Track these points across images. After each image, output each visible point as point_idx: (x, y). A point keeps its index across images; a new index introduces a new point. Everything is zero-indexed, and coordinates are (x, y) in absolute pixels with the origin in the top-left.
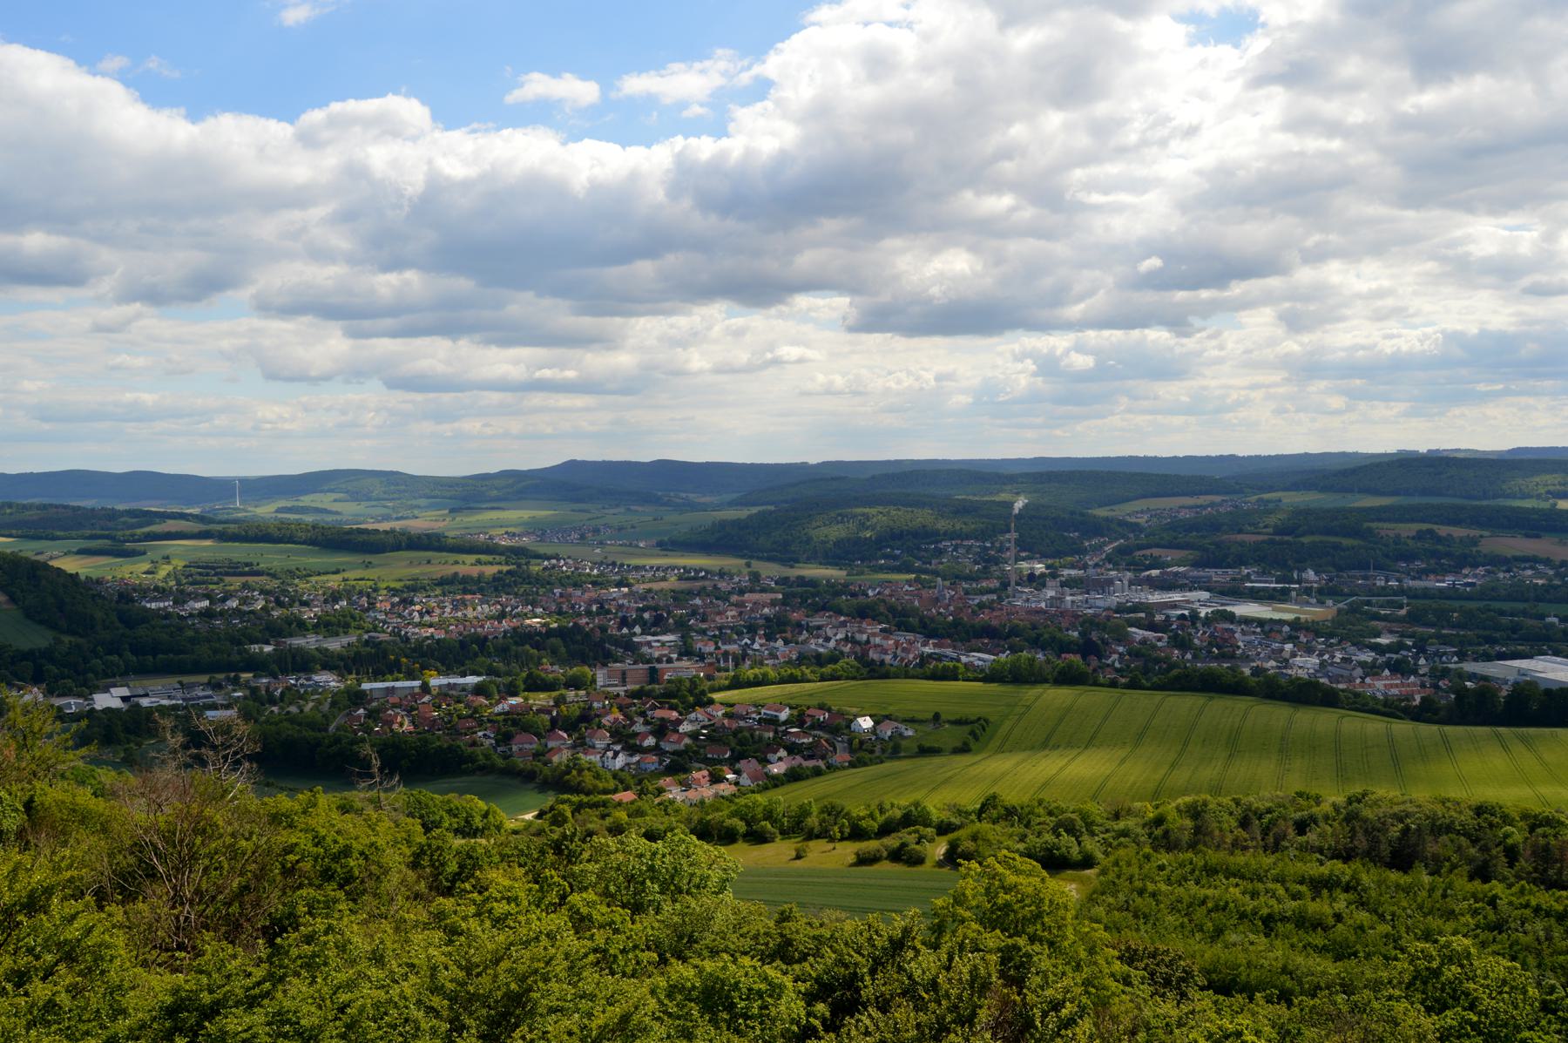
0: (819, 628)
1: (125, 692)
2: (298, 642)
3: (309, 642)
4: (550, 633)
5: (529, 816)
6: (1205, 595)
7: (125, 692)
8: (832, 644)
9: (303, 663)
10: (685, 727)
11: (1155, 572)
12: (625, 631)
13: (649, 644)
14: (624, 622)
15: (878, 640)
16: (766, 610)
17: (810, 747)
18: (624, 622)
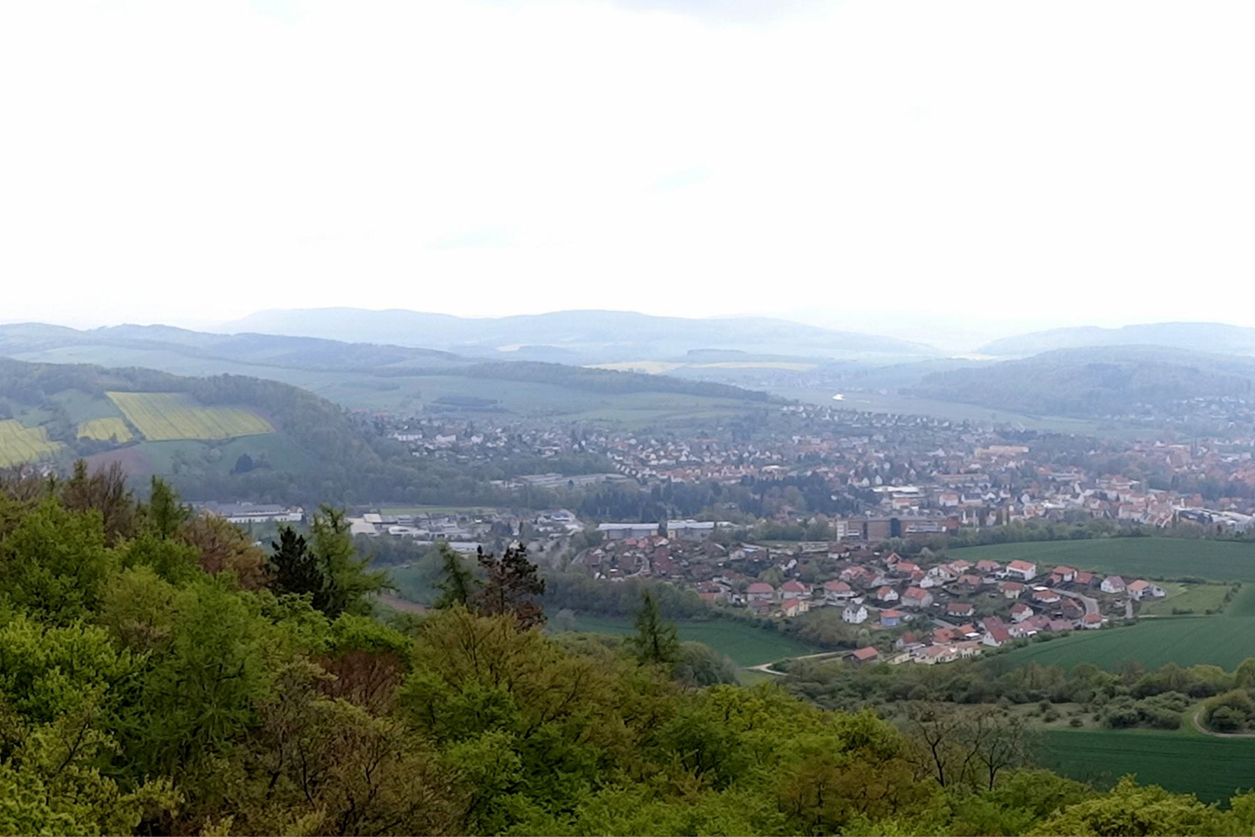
0: (1066, 483)
1: (376, 518)
2: (538, 481)
3: (549, 482)
4: (788, 481)
5: (763, 668)
7: (376, 518)
8: (1080, 500)
9: (543, 502)
10: (927, 582)
12: (866, 482)
13: (890, 495)
14: (865, 473)
15: (1128, 497)
16: (1012, 464)
17: (1057, 606)
18: (865, 473)
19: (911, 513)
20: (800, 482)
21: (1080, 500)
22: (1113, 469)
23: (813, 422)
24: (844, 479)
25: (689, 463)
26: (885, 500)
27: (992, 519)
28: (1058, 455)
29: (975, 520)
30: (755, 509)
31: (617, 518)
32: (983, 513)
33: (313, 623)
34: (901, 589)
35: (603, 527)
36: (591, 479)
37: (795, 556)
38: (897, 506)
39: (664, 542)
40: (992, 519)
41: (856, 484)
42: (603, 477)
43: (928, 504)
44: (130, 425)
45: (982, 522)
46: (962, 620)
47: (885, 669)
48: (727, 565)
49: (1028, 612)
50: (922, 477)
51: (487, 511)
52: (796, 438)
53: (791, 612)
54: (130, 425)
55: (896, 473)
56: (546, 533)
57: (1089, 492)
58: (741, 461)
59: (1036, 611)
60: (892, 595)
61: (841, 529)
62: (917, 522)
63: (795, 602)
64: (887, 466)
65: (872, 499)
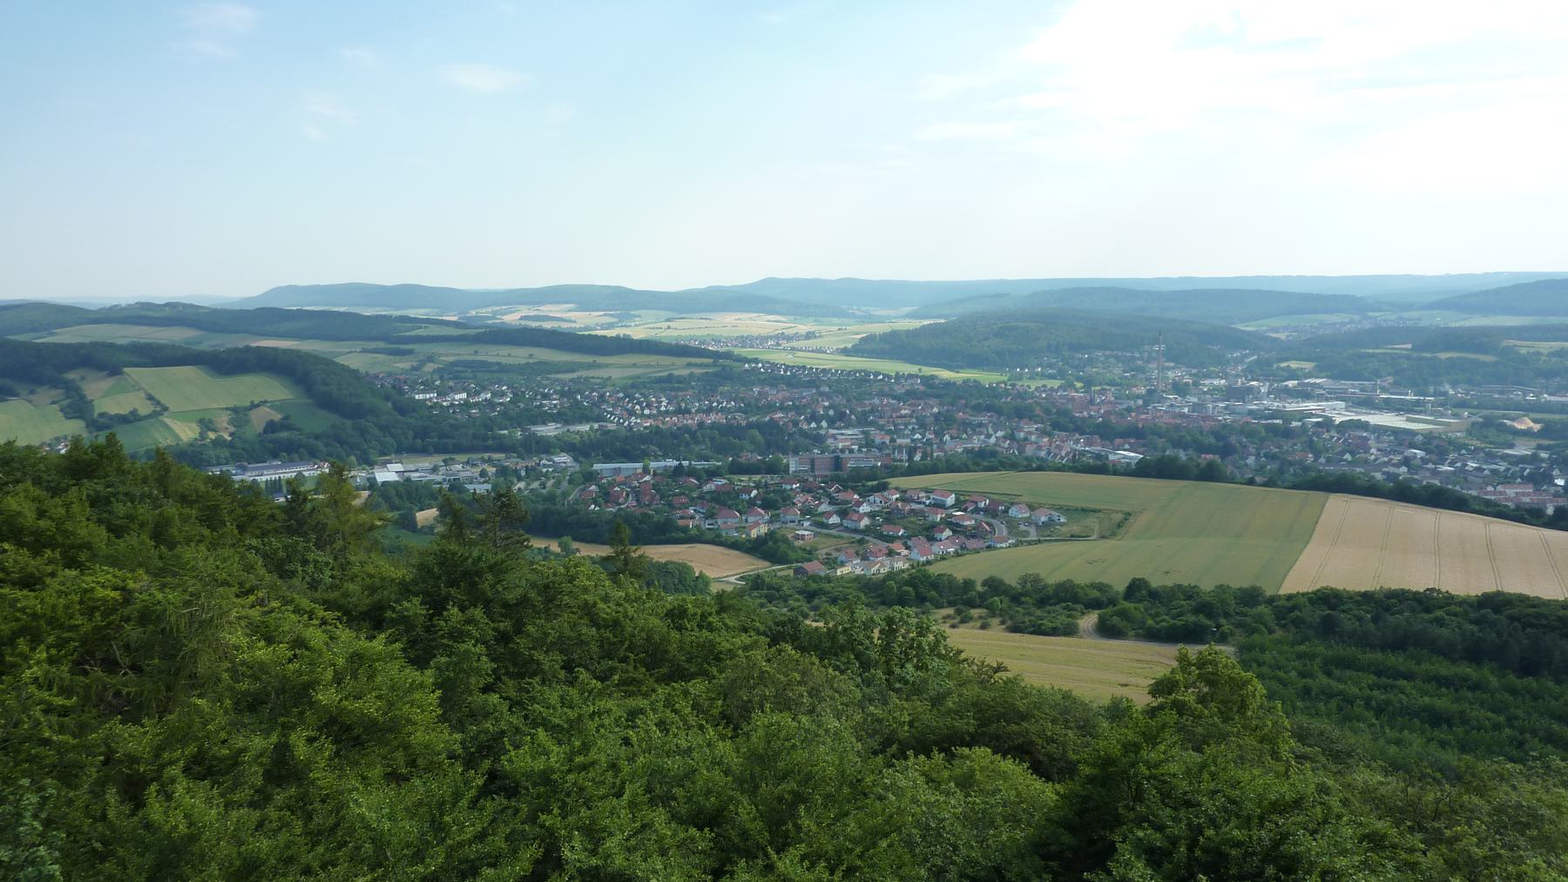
3: (549, 430)
6: (1342, 404)
7: (399, 467)
8: (993, 440)
10: (865, 508)
11: (1291, 384)
12: (813, 425)
13: (834, 436)
14: (814, 417)
19: (851, 451)
20: (758, 426)
21: (993, 440)
22: (1022, 413)
23: (773, 376)
24: (796, 424)
25: (667, 412)
26: (830, 441)
27: (917, 458)
28: (975, 402)
29: (905, 457)
30: (721, 449)
31: (608, 459)
32: (911, 451)
33: (316, 562)
34: (843, 514)
35: (597, 467)
36: (585, 428)
37: (757, 487)
38: (840, 445)
39: (647, 478)
40: (917, 458)
41: (805, 427)
42: (596, 426)
43: (868, 444)
44: (150, 398)
45: (910, 459)
46: (891, 539)
47: (828, 580)
48: (701, 497)
49: (948, 533)
50: (862, 421)
51: (496, 456)
52: (756, 390)
53: (754, 533)
54: (150, 398)
55: (839, 419)
56: (546, 475)
57: (1000, 434)
58: (710, 410)
59: (954, 532)
60: (835, 519)
61: (793, 464)
62: (858, 459)
63: (757, 524)
64: (831, 412)
65: (818, 440)
